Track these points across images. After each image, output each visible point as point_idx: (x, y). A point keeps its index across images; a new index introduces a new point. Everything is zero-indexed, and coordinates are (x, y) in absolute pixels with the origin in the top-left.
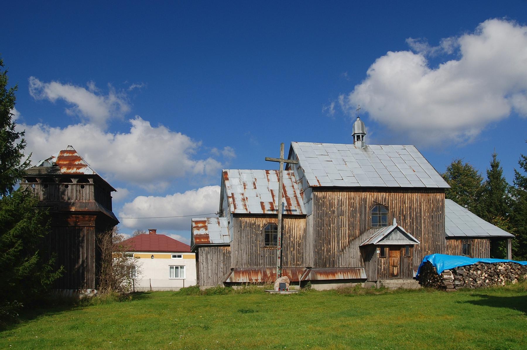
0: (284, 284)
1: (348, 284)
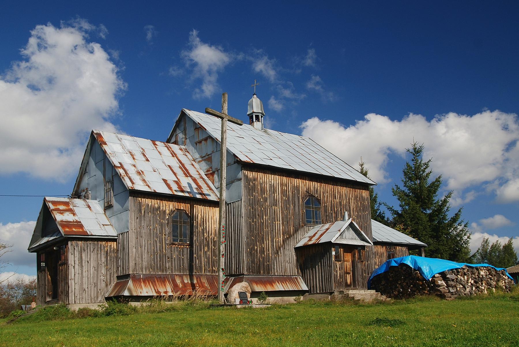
0: (244, 293)
1: (286, 298)
